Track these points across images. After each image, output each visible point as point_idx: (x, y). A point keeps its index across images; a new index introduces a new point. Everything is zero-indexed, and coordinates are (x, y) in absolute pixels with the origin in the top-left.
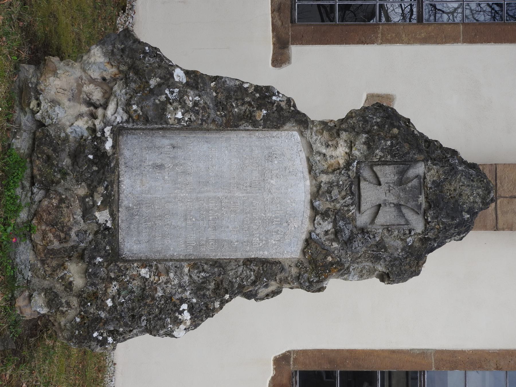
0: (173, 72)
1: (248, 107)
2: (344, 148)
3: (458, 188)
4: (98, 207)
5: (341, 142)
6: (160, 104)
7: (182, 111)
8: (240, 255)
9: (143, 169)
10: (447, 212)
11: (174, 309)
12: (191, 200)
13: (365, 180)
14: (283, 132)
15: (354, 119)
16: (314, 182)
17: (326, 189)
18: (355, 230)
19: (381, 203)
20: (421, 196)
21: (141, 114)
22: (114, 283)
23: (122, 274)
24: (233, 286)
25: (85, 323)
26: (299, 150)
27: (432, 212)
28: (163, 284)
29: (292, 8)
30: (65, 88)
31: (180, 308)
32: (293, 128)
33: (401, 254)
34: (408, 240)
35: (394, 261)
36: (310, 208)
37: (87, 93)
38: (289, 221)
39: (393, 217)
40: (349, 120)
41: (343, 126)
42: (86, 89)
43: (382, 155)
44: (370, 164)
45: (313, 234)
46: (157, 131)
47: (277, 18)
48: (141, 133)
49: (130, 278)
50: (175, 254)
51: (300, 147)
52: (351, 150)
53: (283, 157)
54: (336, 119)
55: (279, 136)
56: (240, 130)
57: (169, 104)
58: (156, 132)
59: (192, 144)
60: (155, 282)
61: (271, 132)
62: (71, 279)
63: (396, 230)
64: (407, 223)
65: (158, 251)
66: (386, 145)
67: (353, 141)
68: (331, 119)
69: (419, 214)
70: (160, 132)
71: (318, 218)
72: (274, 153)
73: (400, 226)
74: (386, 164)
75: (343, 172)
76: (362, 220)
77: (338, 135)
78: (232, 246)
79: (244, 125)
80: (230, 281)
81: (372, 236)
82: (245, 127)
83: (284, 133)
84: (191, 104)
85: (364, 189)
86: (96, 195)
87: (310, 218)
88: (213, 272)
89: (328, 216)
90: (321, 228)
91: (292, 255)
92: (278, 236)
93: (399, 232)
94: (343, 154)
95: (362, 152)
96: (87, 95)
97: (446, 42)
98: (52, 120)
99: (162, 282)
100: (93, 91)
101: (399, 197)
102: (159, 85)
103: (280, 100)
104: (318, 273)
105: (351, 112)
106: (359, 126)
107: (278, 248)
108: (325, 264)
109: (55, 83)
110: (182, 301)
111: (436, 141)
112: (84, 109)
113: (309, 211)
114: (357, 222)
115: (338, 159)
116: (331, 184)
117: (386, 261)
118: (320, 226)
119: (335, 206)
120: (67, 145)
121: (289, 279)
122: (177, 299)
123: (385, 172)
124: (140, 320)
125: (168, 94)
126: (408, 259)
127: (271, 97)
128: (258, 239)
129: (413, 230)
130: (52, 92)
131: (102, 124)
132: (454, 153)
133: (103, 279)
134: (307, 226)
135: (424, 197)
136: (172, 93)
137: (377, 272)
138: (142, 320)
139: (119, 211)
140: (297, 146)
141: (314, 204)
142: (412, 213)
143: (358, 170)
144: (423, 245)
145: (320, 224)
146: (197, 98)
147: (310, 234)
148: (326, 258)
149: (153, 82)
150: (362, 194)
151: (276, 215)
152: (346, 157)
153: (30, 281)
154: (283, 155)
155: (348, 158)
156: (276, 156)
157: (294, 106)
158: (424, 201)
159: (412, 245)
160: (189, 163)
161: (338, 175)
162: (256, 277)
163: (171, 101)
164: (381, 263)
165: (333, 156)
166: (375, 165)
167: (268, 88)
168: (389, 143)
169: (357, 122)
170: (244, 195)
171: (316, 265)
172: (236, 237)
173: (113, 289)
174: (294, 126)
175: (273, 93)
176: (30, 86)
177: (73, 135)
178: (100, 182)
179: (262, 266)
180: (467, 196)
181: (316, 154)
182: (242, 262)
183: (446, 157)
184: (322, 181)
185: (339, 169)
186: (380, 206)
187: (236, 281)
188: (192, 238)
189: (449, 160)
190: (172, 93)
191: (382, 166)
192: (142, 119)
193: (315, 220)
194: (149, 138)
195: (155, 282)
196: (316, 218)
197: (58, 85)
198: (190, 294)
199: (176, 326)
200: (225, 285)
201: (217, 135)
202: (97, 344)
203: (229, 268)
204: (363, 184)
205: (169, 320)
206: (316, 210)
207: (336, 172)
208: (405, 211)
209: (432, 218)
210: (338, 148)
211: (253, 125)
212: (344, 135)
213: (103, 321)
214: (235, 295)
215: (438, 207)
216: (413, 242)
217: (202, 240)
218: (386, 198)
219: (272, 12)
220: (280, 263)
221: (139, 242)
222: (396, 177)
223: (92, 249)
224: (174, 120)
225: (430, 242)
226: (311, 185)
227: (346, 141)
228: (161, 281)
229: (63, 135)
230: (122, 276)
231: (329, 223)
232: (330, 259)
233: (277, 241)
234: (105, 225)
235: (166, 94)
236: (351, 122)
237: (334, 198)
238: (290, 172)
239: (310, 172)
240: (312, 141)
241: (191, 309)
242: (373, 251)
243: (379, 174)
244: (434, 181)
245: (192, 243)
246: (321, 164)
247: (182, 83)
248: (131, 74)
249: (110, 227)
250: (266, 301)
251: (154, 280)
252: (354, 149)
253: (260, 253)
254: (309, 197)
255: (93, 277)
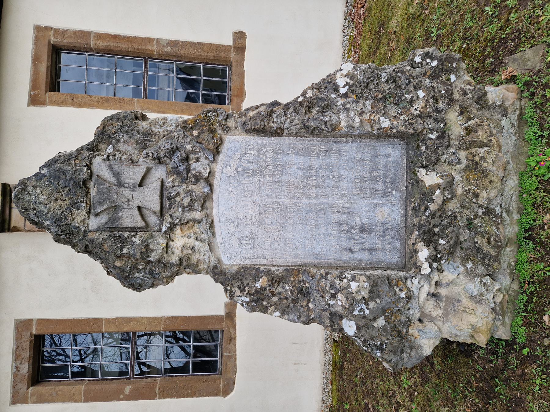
0: (356, 332)
1: (274, 290)
2: (175, 246)
3: (52, 202)
4: (439, 188)
5: (177, 252)
6: (376, 298)
7: (350, 290)
8: (286, 141)
9: (382, 228)
10: (66, 176)
11: (354, 88)
12: (333, 196)
13: (155, 213)
14: (239, 263)
15: (164, 276)
16: (208, 212)
17: (196, 204)
18: (168, 161)
19: (138, 189)
20: (94, 194)
21: (395, 287)
22: (418, 112)
23: (409, 121)
24: (295, 109)
25: (445, 74)
26: (223, 245)
27: (81, 177)
28: (366, 112)
29: (222, 339)
30: (464, 314)
31: (348, 89)
32: (228, 267)
33: (121, 137)
34: (112, 150)
35: (128, 130)
36: (213, 185)
37: (439, 307)
38: (235, 172)
39: (126, 173)
40: (169, 274)
41: (176, 269)
42: (440, 312)
43: (133, 238)
44: (149, 229)
45: (212, 159)
46: (367, 266)
47: (233, 333)
48: (382, 264)
49: (399, 118)
50: (351, 143)
51: (221, 247)
52: (167, 244)
53: (239, 238)
54: (185, 275)
55: (243, 260)
56: (283, 266)
57: (366, 298)
58: (368, 265)
59: (332, 252)
60: (374, 114)
61: (251, 263)
62: (460, 118)
63: (124, 160)
64: (111, 168)
65: (368, 146)
66: (128, 248)
67: (165, 253)
68: (189, 275)
69: (98, 176)
70: (363, 265)
71: (205, 174)
72: (248, 242)
73: (120, 164)
74: (131, 228)
75: (178, 221)
76: (159, 173)
77: (180, 260)
78: (294, 149)
79: (277, 271)
80: (297, 113)
81: (150, 154)
82: (279, 270)
83: (238, 262)
84: (340, 296)
85: (156, 203)
86: (440, 201)
87: (214, 175)
88: (315, 121)
89: (195, 176)
90: (203, 165)
91: (233, 138)
92: (247, 158)
93: (121, 158)
94: (176, 241)
95: (155, 242)
96: (439, 305)
97: (116, 319)
98: (481, 281)
99: (366, 114)
100: (433, 309)
101: (118, 194)
102: (375, 319)
103: (241, 297)
104: (208, 120)
105: (168, 282)
106: (159, 269)
107: (248, 147)
108: (200, 128)
109: (477, 320)
110: (345, 96)
111: (78, 252)
112: (443, 291)
113: (215, 182)
114: (165, 170)
115: (182, 235)
116: (191, 208)
117: (137, 131)
118: (204, 167)
119: (188, 187)
120: (463, 255)
121: (237, 116)
122: (350, 97)
123: (132, 220)
124: (388, 78)
125: (365, 309)
126: (113, 131)
127: (251, 301)
128: (268, 156)
129: (104, 160)
130: (480, 310)
131: (431, 276)
132: (57, 240)
133: (429, 117)
134: (217, 168)
135: (91, 193)
136: (361, 310)
137: (148, 122)
138: (386, 78)
139: (406, 187)
140: (225, 248)
141: (209, 189)
142: (105, 177)
143: (162, 224)
144: (97, 145)
145: (204, 169)
146: (332, 302)
147: (214, 159)
148: (199, 134)
149: (381, 322)
150: (158, 198)
151: (248, 180)
152: (173, 236)
153: (503, 116)
154: (239, 240)
155: (171, 236)
156: (247, 239)
157: (226, 290)
158: (92, 189)
159: (108, 145)
160: (335, 233)
161: (183, 218)
162: (271, 116)
163: (364, 301)
164: (142, 129)
165: (187, 238)
166: (143, 228)
167: (253, 310)
168: (125, 251)
169: (161, 273)
170: (281, 200)
171: (210, 127)
172: (290, 159)
173: (418, 106)
174: (227, 269)
175: (248, 305)
176: (500, 317)
177: (456, 264)
178: (433, 215)
179: (265, 126)
180: (43, 193)
181: (206, 240)
182: (285, 133)
183: (66, 235)
184: (200, 212)
185: (182, 224)
186: (140, 185)
187: (291, 113)
188: (334, 159)
189: (62, 232)
190: (361, 310)
191: (136, 227)
192: (394, 282)
193: (209, 173)
194: (375, 260)
195: (374, 114)
196: (207, 175)
197: (473, 317)
198: (337, 102)
199: (351, 73)
200: (303, 110)
201: (306, 261)
202: (432, 54)
203: (298, 126)
204: (157, 208)
205: (359, 77)
206: (207, 183)
207: (185, 221)
208: (113, 180)
209: (82, 171)
210: (182, 246)
211: (270, 271)
212: (175, 259)
213: (427, 76)
214: (291, 103)
215: (75, 182)
216: (107, 148)
217: (323, 156)
218: (132, 193)
219: (235, 337)
220: (246, 131)
221: (386, 156)
222: (120, 214)
223: (441, 147)
224: (359, 279)
225: (88, 147)
226: (211, 208)
227: (173, 253)
228: (368, 114)
229: (469, 265)
230: (408, 120)
231: (195, 169)
232: (195, 133)
233: (248, 153)
234: (427, 171)
235: (368, 309)
236: (167, 273)
237: (188, 194)
238: (233, 222)
239: (212, 222)
240: (209, 253)
241: (336, 89)
242: (150, 141)
243: (139, 218)
244: (78, 209)
245: (334, 153)
246: (200, 230)
247: (347, 319)
248: (405, 332)
249: (421, 169)
250: (258, 104)
251: (375, 116)
252: (165, 245)
253: (265, 142)
254: (214, 196)
255: (440, 119)
